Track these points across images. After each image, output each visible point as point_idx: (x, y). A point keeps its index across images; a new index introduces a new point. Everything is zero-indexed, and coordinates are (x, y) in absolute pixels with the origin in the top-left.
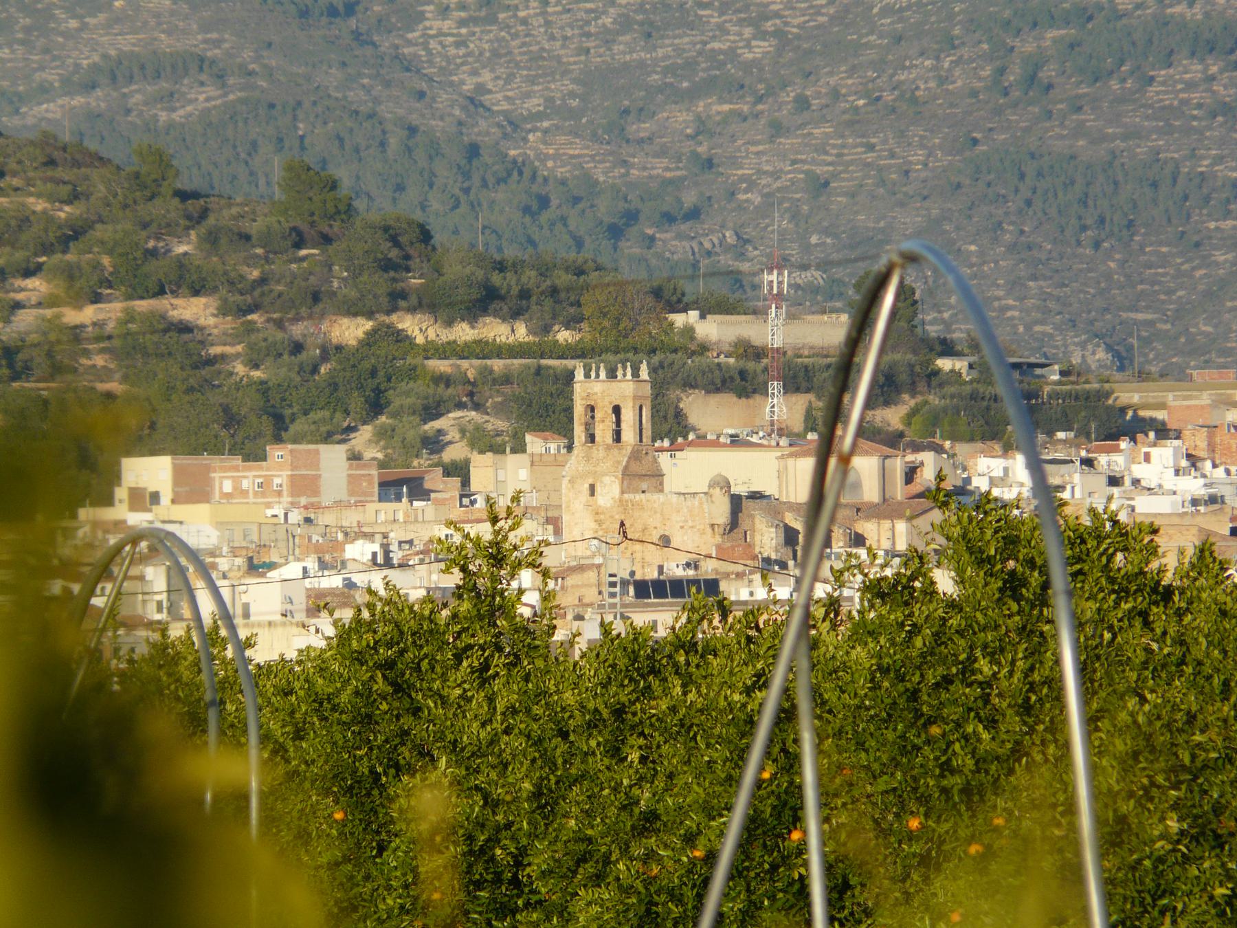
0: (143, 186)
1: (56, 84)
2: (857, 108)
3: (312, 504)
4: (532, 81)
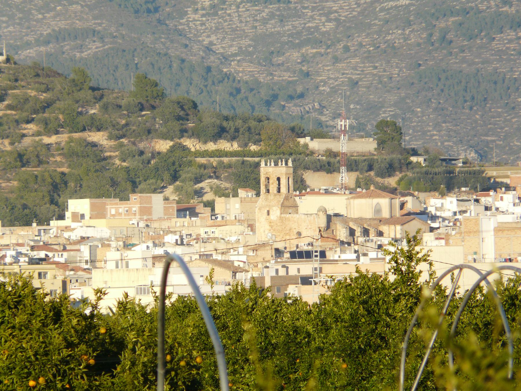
0: (76, 85)
1: (33, 42)
2: (370, 51)
3: (149, 219)
4: (233, 40)
